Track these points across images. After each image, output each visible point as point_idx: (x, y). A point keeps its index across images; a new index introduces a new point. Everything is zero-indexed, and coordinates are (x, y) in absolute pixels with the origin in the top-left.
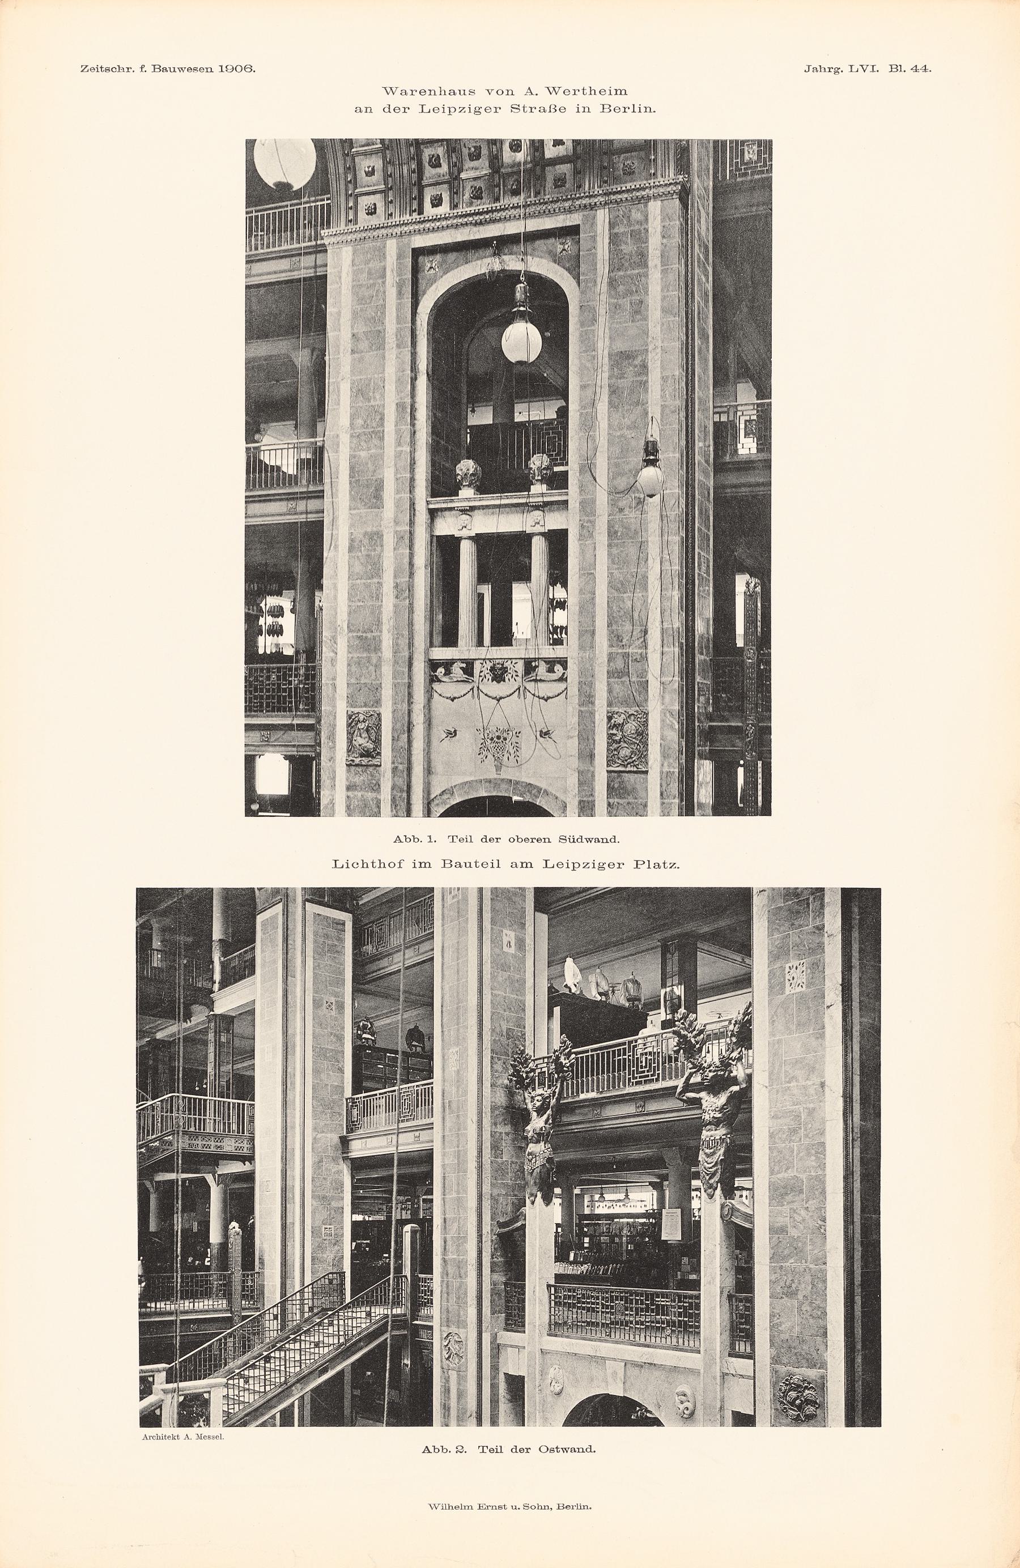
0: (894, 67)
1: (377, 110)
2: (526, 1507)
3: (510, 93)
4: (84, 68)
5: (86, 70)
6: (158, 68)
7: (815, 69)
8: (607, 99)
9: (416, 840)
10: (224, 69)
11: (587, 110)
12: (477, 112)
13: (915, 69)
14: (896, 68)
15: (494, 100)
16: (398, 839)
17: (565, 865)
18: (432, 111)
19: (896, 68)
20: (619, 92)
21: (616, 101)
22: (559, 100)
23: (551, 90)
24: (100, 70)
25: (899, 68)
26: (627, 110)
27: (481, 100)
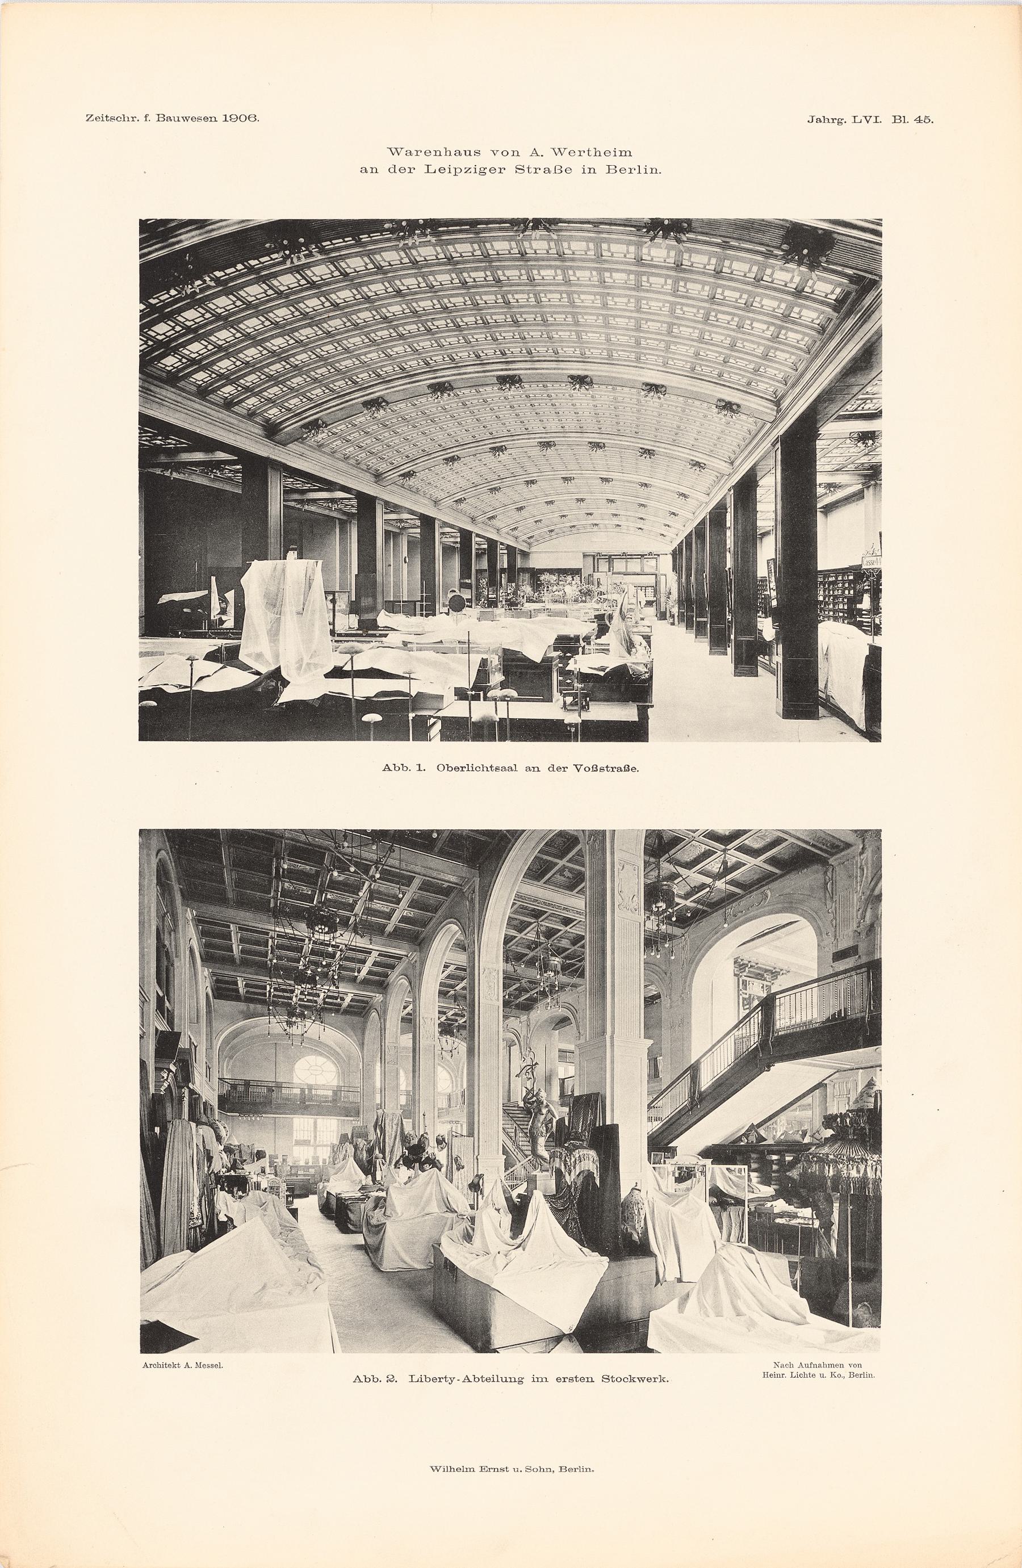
0: (897, 118)
1: (383, 170)
2: (528, 1469)
3: (516, 153)
4: (89, 117)
5: (91, 119)
6: (163, 118)
7: (819, 120)
8: (611, 160)
9: (405, 769)
10: (228, 118)
11: (592, 171)
12: (482, 173)
13: (919, 120)
14: (899, 119)
15: (498, 161)
16: (387, 768)
17: (447, 170)
18: (437, 171)
19: (899, 119)
20: (623, 154)
21: (621, 162)
22: (564, 161)
23: (557, 151)
24: (105, 119)
25: (902, 119)
26: (633, 171)
27: (486, 160)
